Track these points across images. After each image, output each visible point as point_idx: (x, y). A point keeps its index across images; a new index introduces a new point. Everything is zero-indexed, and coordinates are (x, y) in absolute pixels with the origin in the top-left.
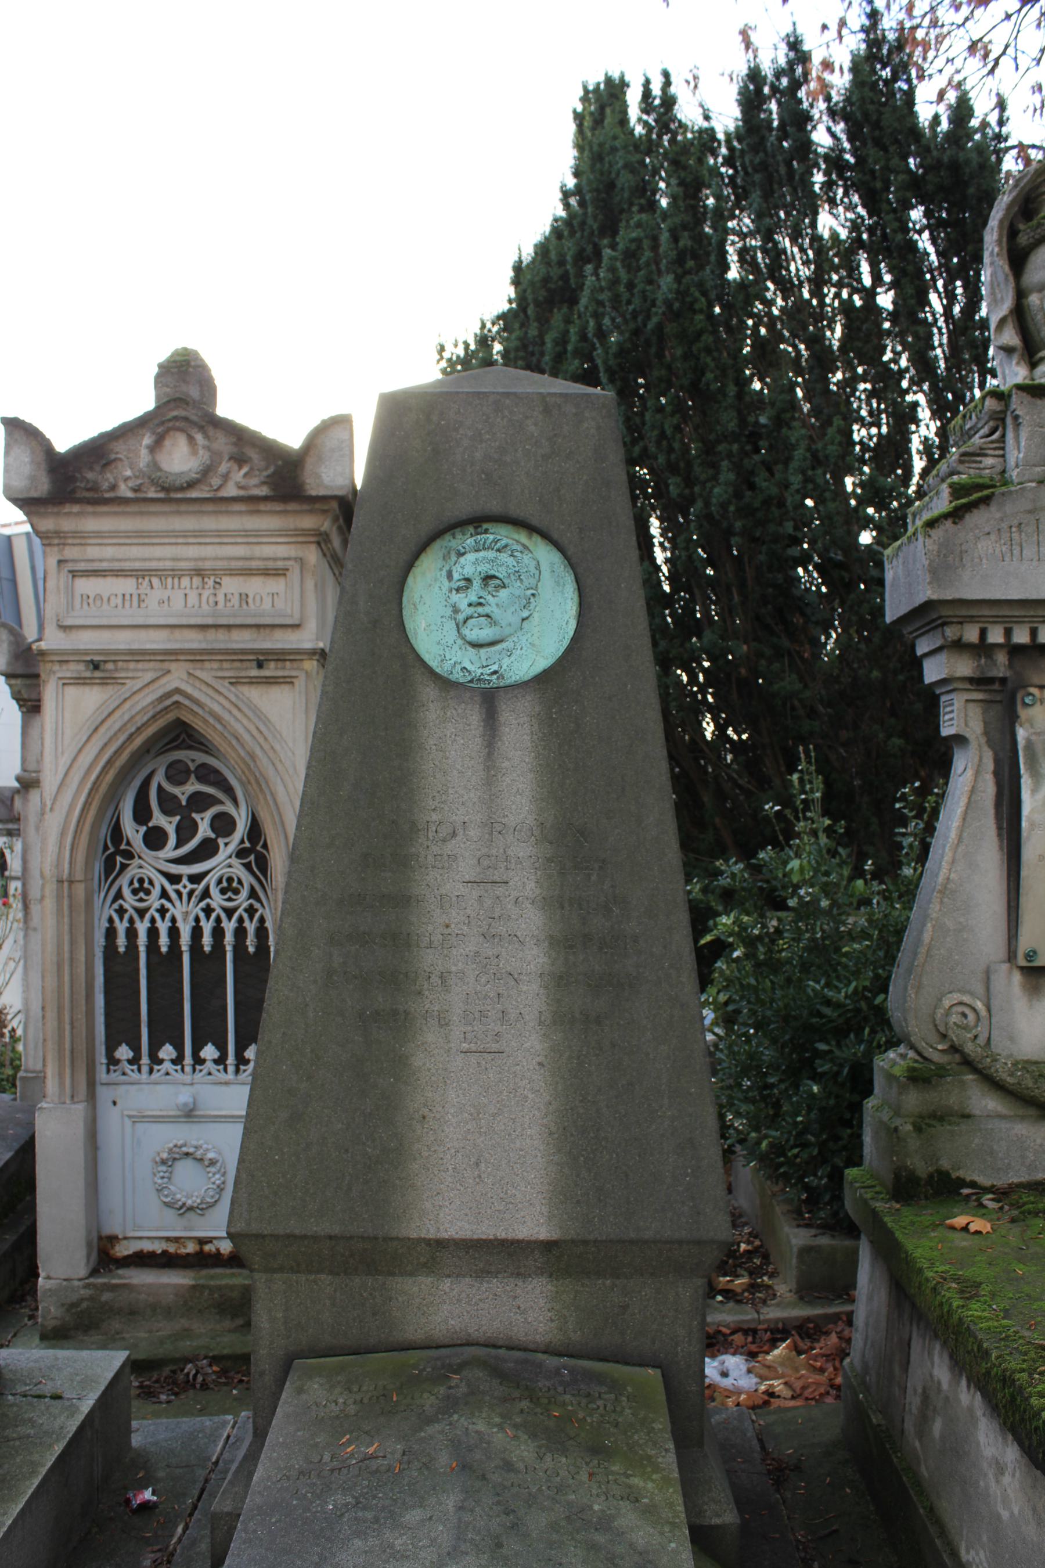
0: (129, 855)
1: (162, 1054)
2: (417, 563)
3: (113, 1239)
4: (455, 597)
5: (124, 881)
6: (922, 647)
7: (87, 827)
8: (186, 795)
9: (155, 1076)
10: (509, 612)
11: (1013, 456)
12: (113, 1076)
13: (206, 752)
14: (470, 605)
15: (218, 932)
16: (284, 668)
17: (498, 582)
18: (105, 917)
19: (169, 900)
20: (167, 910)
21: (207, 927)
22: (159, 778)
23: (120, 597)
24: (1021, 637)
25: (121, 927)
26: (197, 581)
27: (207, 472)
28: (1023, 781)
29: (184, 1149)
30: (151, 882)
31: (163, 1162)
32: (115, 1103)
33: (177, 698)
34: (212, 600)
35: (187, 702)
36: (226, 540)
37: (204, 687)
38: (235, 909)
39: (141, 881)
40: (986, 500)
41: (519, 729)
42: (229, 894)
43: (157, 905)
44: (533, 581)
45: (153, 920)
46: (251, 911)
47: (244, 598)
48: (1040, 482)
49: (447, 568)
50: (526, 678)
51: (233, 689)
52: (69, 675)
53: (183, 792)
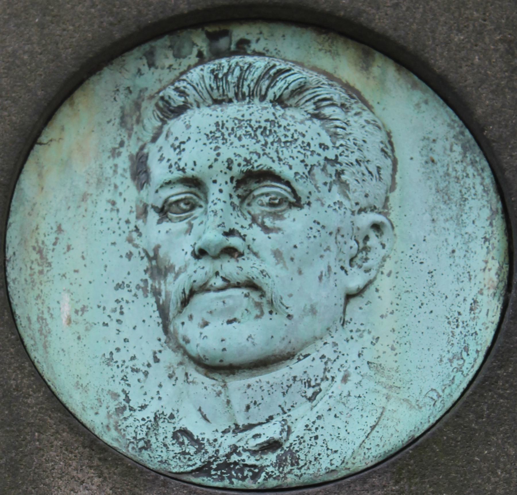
2: (49, 133)
4: (157, 232)
10: (311, 274)
14: (201, 254)
17: (281, 190)
44: (376, 189)
50: (360, 464)
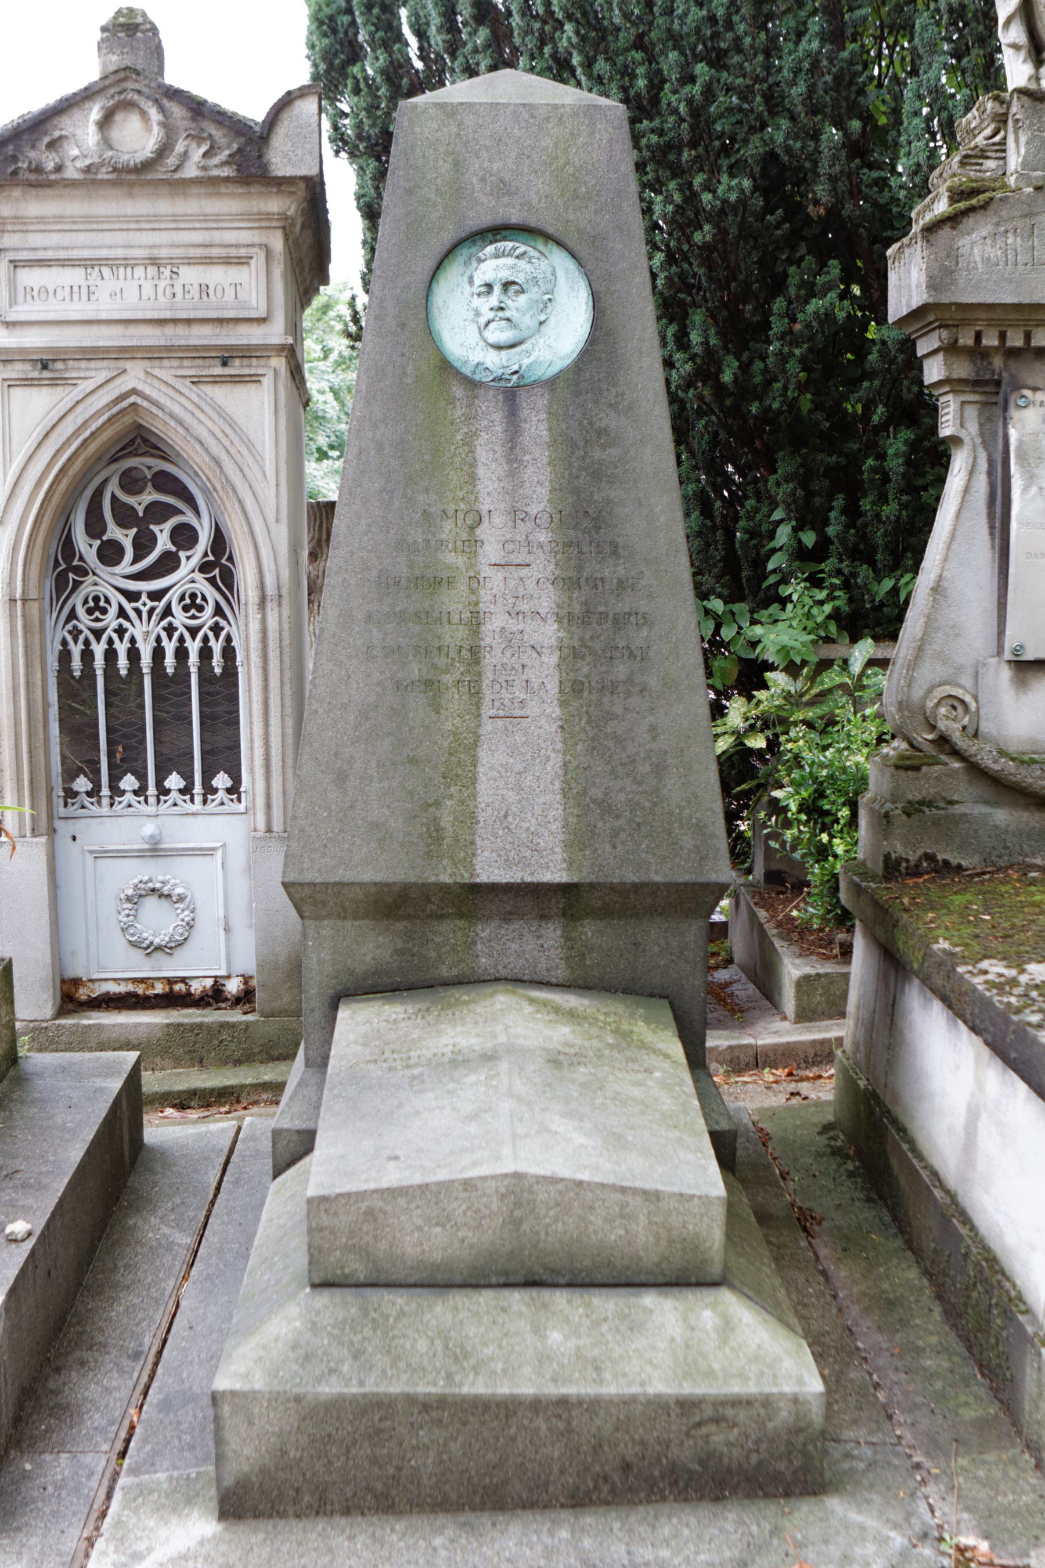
0: (83, 572)
1: (123, 785)
3: (77, 982)
4: (477, 302)
5: (77, 599)
6: (922, 348)
7: (40, 541)
8: (143, 506)
9: (117, 807)
11: (1014, 161)
12: (72, 810)
13: (164, 458)
15: (181, 653)
16: (250, 366)
17: (516, 287)
18: (58, 639)
19: (127, 618)
20: (126, 630)
21: (170, 647)
22: (113, 487)
23: (67, 289)
24: (1016, 340)
25: (76, 650)
26: (152, 270)
27: (163, 151)
28: (1013, 481)
29: (150, 885)
30: (107, 601)
31: (129, 899)
32: (74, 838)
33: (133, 399)
34: (169, 291)
35: (145, 404)
36: (182, 225)
37: (163, 388)
38: (199, 628)
39: (96, 599)
40: (985, 206)
41: (537, 426)
42: (193, 611)
43: (114, 625)
44: (549, 286)
45: (110, 642)
46: (216, 629)
47: (204, 289)
48: (1038, 189)
49: (468, 273)
50: (544, 378)
51: (194, 387)
52: (14, 375)
53: (140, 502)
